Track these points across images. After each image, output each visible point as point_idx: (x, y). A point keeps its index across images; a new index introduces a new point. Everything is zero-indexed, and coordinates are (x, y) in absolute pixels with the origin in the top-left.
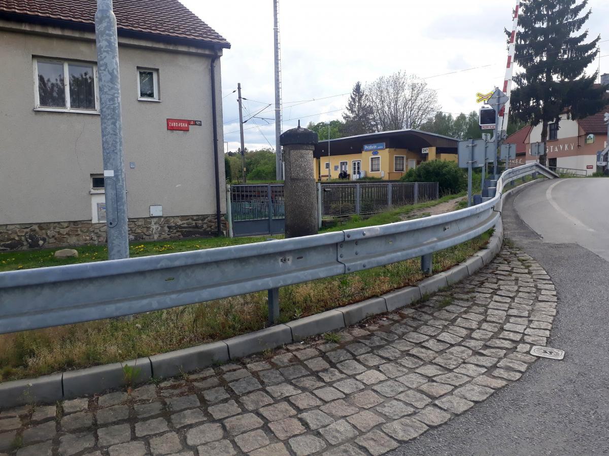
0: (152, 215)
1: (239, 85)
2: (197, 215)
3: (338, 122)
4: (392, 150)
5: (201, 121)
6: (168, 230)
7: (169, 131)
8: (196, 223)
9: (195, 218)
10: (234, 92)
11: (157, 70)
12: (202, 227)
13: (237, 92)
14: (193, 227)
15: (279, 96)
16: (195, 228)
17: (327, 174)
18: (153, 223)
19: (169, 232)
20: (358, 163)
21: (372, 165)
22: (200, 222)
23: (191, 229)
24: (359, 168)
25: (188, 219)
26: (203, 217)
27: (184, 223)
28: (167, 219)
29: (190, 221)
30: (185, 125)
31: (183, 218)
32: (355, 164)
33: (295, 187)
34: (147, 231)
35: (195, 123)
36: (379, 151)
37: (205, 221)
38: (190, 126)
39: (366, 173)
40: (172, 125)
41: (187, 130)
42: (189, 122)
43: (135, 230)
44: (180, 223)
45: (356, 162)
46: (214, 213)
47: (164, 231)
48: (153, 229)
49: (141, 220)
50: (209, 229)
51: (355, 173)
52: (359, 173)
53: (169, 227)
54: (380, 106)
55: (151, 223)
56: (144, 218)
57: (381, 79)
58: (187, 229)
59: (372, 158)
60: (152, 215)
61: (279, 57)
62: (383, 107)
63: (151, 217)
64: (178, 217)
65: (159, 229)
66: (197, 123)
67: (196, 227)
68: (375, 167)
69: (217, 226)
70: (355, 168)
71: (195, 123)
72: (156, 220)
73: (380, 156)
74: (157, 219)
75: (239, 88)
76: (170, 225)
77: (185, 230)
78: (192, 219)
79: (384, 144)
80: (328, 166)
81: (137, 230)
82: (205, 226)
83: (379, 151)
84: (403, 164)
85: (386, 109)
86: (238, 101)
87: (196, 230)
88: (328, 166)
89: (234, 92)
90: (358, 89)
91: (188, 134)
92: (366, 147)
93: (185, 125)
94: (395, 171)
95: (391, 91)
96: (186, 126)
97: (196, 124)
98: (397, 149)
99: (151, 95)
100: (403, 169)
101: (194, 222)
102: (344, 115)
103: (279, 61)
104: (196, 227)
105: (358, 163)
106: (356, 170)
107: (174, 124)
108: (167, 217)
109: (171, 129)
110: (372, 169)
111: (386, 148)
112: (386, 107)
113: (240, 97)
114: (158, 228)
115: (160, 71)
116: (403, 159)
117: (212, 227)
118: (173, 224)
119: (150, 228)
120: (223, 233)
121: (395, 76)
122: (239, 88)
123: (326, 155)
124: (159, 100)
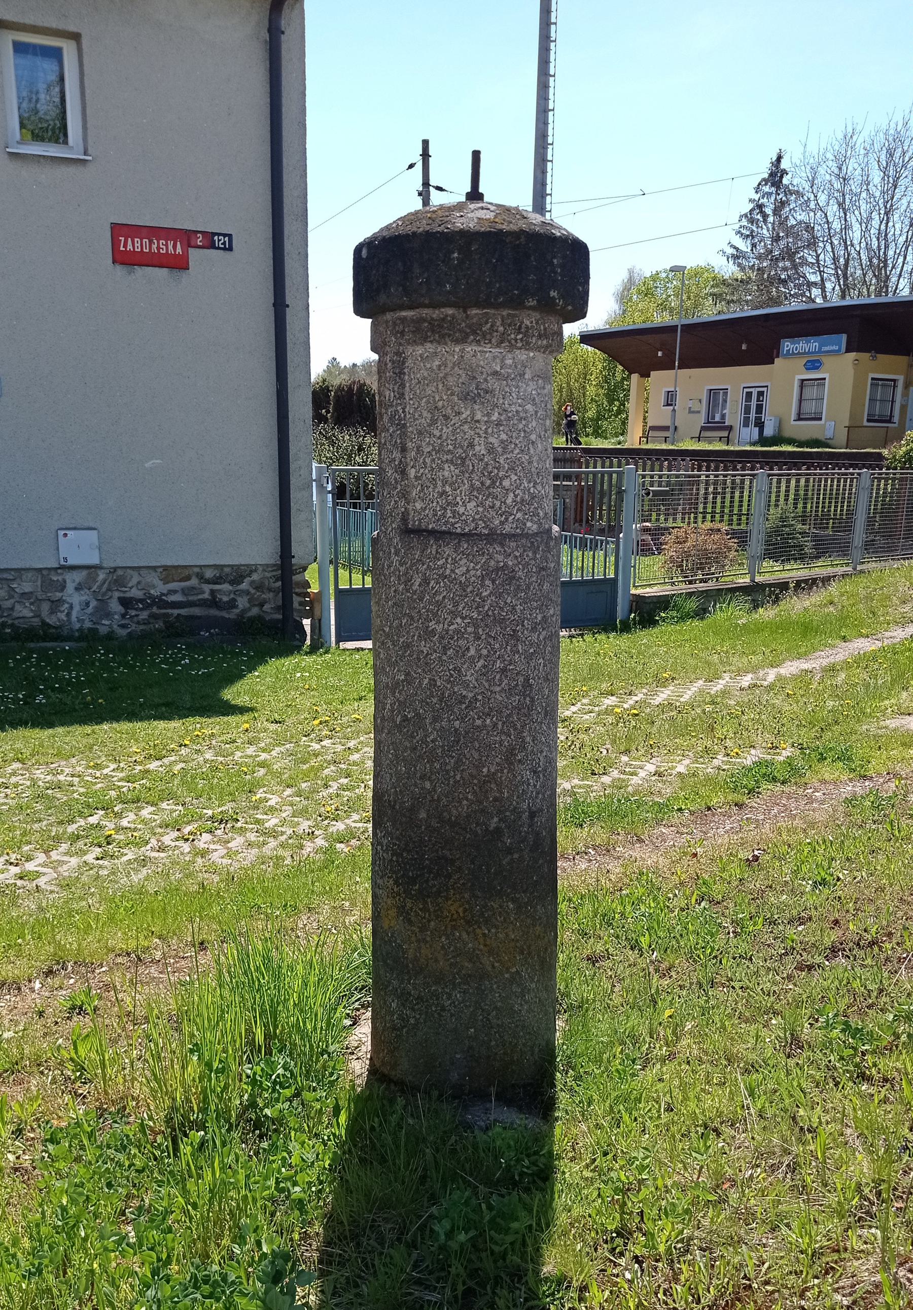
0: (65, 559)
1: (426, 143)
2: (215, 566)
3: (709, 269)
4: (865, 356)
5: (230, 236)
6: (120, 609)
7: (118, 267)
8: (213, 592)
9: (209, 574)
10: (411, 166)
11: (76, 37)
12: (232, 604)
13: (419, 167)
14: (203, 603)
15: (544, 184)
16: (210, 607)
17: (667, 422)
18: (70, 587)
19: (123, 616)
20: (761, 394)
21: (800, 401)
22: (226, 587)
23: (196, 611)
24: (759, 409)
25: (188, 578)
26: (238, 574)
27: (175, 592)
28: (118, 577)
29: (194, 582)
30: (175, 247)
31: (169, 573)
32: (749, 395)
33: (426, 581)
34: (53, 612)
35: (210, 241)
36: (824, 359)
37: (244, 586)
38: (191, 250)
39: (780, 425)
40: (130, 247)
41: (179, 264)
42: (187, 237)
43: (12, 609)
44: (159, 588)
45: (755, 392)
46: (272, 562)
47: (108, 615)
48: (71, 607)
49: (30, 575)
50: (255, 611)
51: (746, 424)
52: (760, 424)
53: (126, 603)
54: (836, 226)
55: (63, 587)
56: (40, 570)
57: (848, 139)
58: (183, 612)
59: (803, 380)
60: (65, 559)
61: (552, 65)
62: (847, 227)
63: (62, 567)
64: (154, 568)
65: (90, 610)
66: (219, 241)
67: (213, 602)
68: (810, 408)
69: (280, 603)
70: (747, 410)
71: (210, 241)
72: (77, 577)
73: (826, 375)
74: (85, 573)
75: (425, 155)
76: (128, 595)
77: (176, 612)
78: (201, 577)
79: (844, 337)
80: (670, 399)
81: (18, 607)
82: (242, 602)
83: (824, 359)
84: (893, 401)
85: (856, 234)
86: (420, 194)
87: (214, 612)
88: (670, 399)
89: (411, 166)
90: (776, 176)
91: (184, 276)
92: (787, 345)
93: (175, 247)
94: (868, 421)
95: (876, 177)
96: (179, 250)
97: (212, 246)
98: (880, 356)
99: (59, 134)
100: (891, 416)
101: (207, 588)
102: (730, 251)
103: (551, 79)
104: (213, 602)
105: (761, 394)
106: (753, 415)
107: (136, 245)
108: (115, 569)
109: (123, 259)
110: (799, 414)
111: (848, 350)
112: (856, 226)
113: (426, 184)
114: (87, 604)
115: (85, 42)
116: (895, 386)
117: (266, 607)
118: (136, 593)
119: (61, 601)
120: (302, 626)
121: (892, 132)
122: (425, 155)
123: (667, 365)
124: (85, 154)
